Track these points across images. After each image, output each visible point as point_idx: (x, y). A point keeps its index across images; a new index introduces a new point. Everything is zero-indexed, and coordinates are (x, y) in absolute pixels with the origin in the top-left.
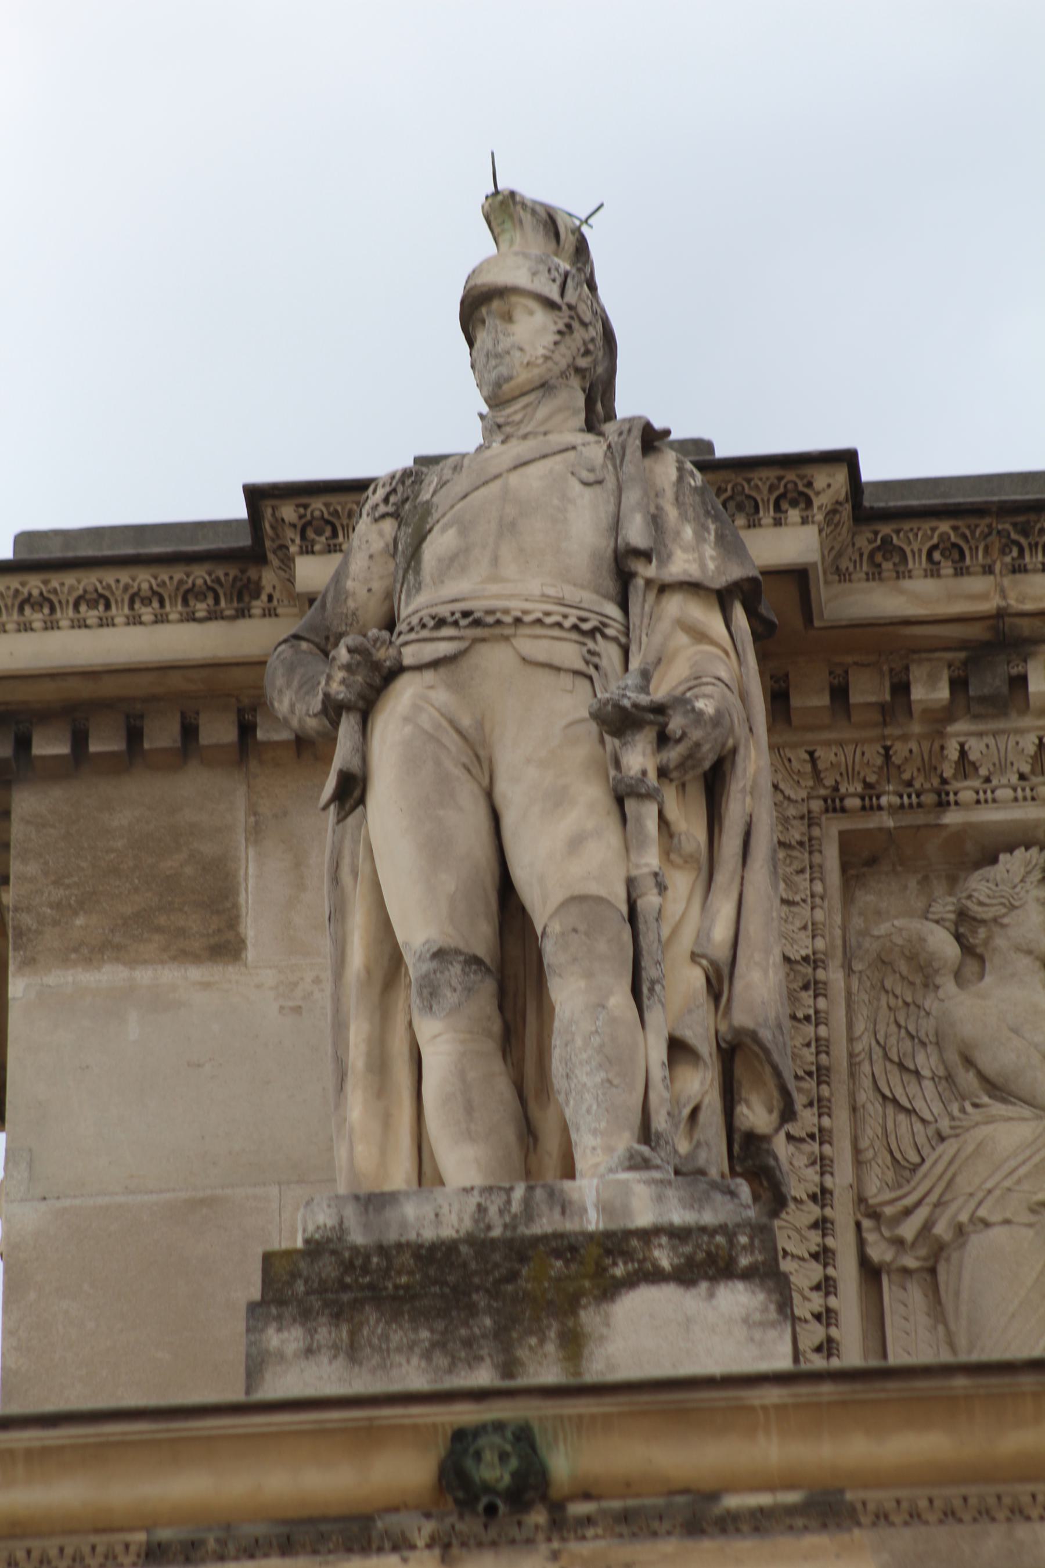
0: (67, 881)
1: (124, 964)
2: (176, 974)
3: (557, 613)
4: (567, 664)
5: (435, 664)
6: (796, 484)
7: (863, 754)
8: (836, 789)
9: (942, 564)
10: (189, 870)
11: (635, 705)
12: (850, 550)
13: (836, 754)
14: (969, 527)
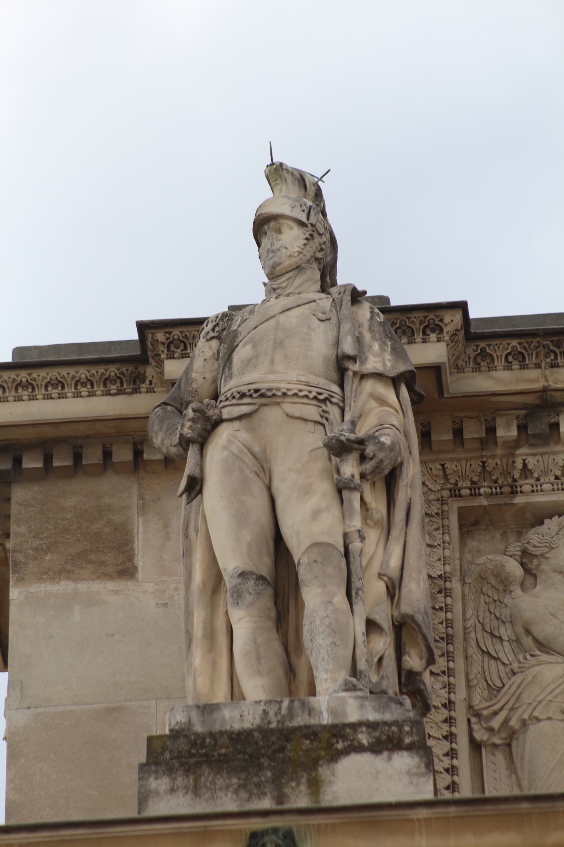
0: (41, 536)
1: (72, 581)
3: (306, 390)
5: (239, 418)
6: (434, 320)
7: (471, 465)
8: (456, 485)
9: (513, 363)
11: (348, 440)
13: (456, 466)
14: (527, 343)
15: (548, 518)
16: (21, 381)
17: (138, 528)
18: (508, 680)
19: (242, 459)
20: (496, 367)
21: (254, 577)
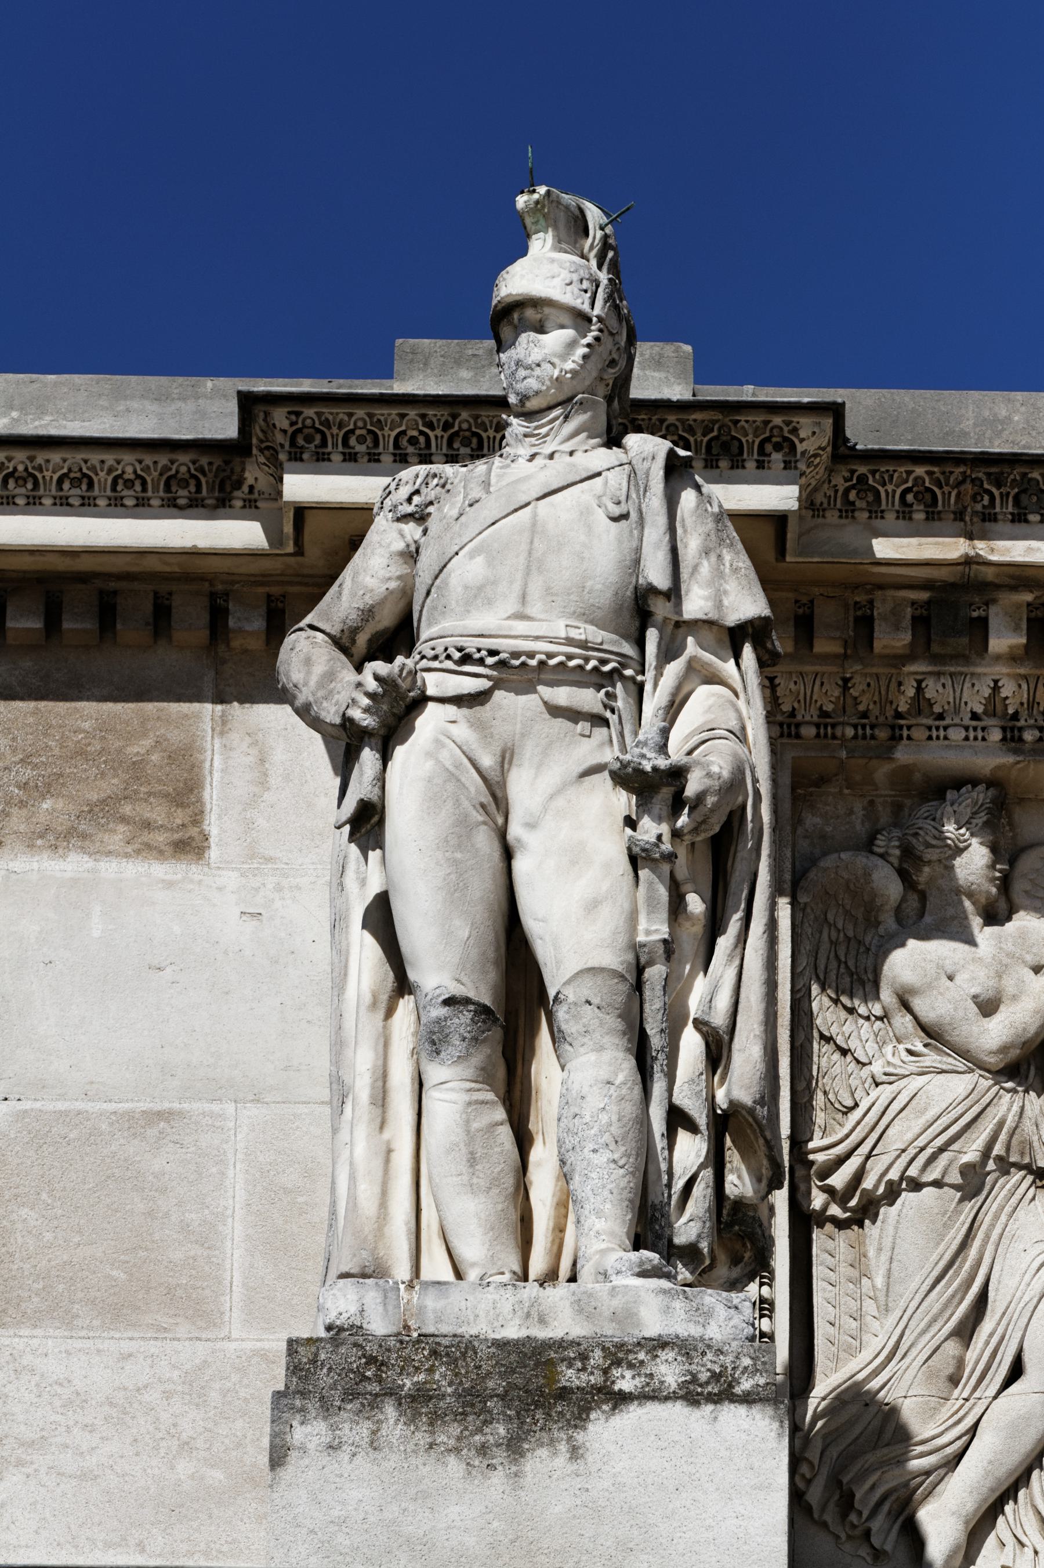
0: (35, 760)
1: (90, 855)
2: (139, 869)
3: (579, 657)
4: (586, 708)
5: (458, 700)
6: (781, 429)
7: (822, 684)
8: (793, 714)
9: (915, 507)
10: (155, 757)
11: (655, 769)
12: (826, 486)
13: (796, 683)
14: (943, 473)
15: (953, 788)
16: (15, 469)
17: (212, 760)
18: (864, 1094)
19: (459, 780)
20: (882, 511)
21: (472, 1007)
